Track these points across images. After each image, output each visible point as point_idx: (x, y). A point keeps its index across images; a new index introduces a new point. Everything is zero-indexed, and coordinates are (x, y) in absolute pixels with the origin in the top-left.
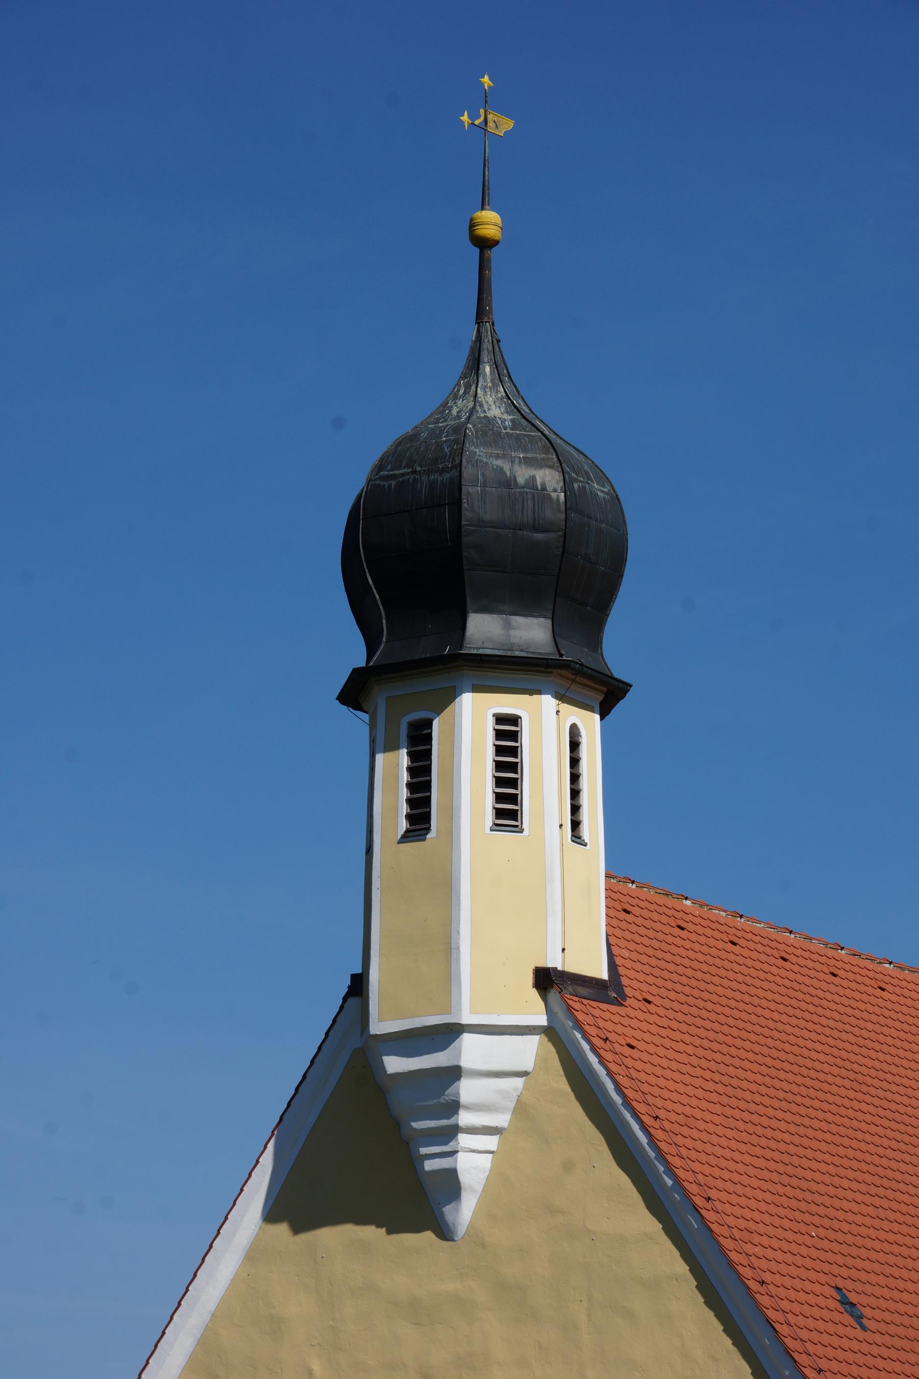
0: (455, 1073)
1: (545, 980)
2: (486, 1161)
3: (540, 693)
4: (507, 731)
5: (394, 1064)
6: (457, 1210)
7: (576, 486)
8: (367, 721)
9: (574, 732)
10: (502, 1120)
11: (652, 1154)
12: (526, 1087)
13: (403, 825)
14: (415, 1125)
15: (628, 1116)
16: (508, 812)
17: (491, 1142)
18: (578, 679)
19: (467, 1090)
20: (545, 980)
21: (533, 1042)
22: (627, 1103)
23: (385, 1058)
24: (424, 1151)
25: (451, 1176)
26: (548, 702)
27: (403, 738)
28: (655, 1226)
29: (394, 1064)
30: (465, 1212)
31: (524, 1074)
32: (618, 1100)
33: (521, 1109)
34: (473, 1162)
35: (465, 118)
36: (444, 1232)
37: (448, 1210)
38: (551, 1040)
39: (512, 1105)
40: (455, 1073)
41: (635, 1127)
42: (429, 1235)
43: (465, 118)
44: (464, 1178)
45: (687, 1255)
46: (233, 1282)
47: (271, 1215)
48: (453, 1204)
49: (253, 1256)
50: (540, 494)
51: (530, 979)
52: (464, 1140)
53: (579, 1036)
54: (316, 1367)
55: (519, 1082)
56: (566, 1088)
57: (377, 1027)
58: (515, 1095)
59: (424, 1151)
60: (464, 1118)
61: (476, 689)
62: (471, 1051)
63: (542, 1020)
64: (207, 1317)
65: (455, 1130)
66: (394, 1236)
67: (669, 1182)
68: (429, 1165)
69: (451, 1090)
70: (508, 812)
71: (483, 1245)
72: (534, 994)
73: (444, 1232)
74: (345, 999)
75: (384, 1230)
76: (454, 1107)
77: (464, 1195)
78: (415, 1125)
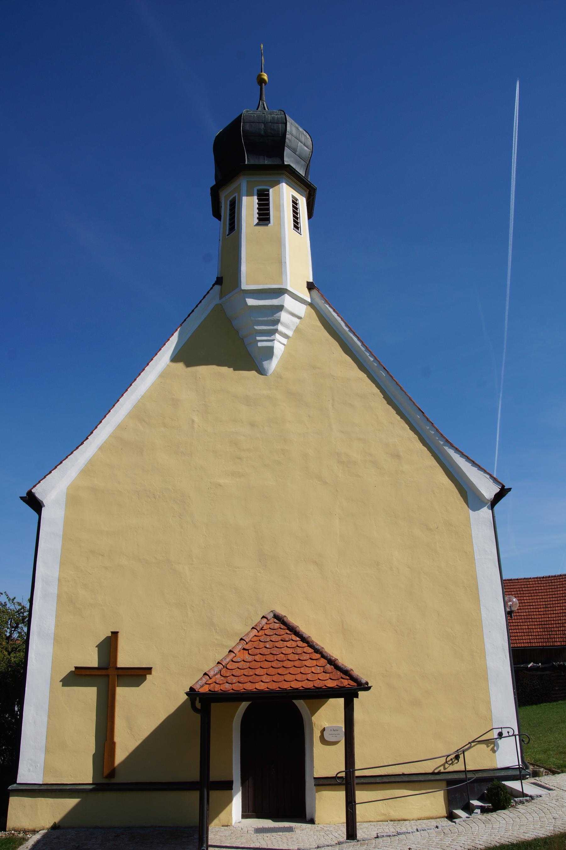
0: (280, 308)
5: (251, 302)
6: (270, 364)
8: (287, 151)
11: (363, 349)
12: (300, 323)
13: (256, 221)
14: (256, 327)
15: (352, 335)
16: (297, 226)
19: (284, 316)
22: (351, 330)
23: (247, 299)
24: (258, 338)
25: (271, 349)
27: (255, 192)
28: (364, 376)
29: (251, 302)
30: (273, 365)
31: (300, 318)
32: (347, 329)
33: (297, 330)
34: (279, 346)
36: (262, 372)
37: (265, 363)
38: (312, 307)
39: (294, 329)
40: (280, 308)
41: (355, 339)
42: (254, 373)
44: (276, 351)
45: (378, 386)
46: (153, 385)
47: (175, 359)
48: (268, 361)
49: (163, 375)
51: (305, 285)
52: (277, 336)
53: (327, 306)
54: (196, 419)
55: (297, 321)
56: (319, 324)
57: (244, 286)
58: (296, 325)
59: (258, 338)
60: (280, 327)
61: (286, 183)
62: (287, 301)
64: (139, 397)
65: (276, 331)
66: (236, 372)
67: (372, 359)
68: (260, 344)
69: (277, 315)
70: (297, 226)
71: (281, 378)
72: (307, 290)
73: (262, 372)
74: (213, 285)
75: (232, 369)
76: (277, 322)
77: (274, 358)
78: (256, 327)
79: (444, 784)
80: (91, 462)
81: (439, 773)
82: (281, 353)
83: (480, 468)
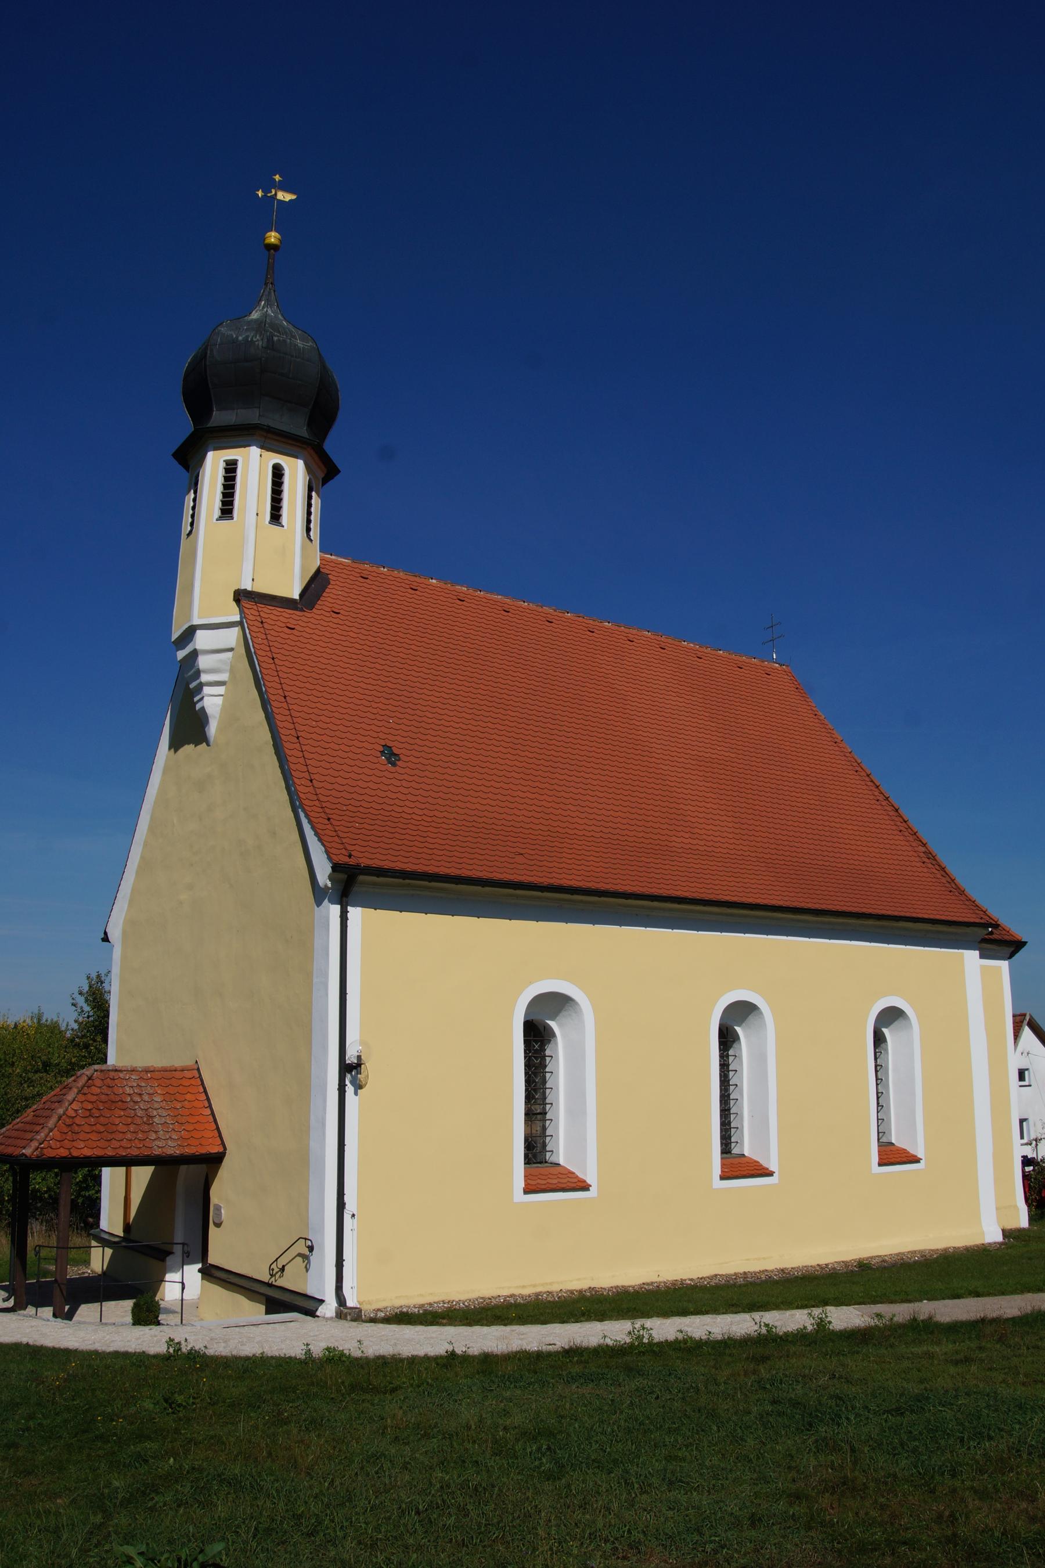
1: (241, 596)
2: (219, 701)
3: (297, 457)
4: (231, 468)
7: (275, 338)
9: (278, 473)
10: (224, 677)
16: (227, 511)
17: (221, 690)
18: (270, 435)
19: (203, 662)
20: (241, 596)
21: (236, 631)
26: (254, 451)
31: (231, 650)
35: (260, 193)
39: (228, 668)
40: (195, 654)
43: (260, 193)
44: (208, 711)
47: (175, 745)
50: (248, 343)
52: (206, 690)
55: (230, 654)
60: (204, 678)
61: (215, 449)
62: (202, 640)
63: (237, 618)
70: (227, 511)
76: (198, 673)
79: (264, 1299)
80: (134, 890)
81: (270, 1285)
82: (218, 709)
83: (320, 840)
